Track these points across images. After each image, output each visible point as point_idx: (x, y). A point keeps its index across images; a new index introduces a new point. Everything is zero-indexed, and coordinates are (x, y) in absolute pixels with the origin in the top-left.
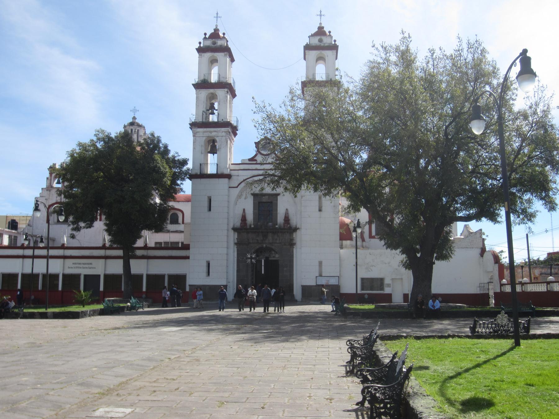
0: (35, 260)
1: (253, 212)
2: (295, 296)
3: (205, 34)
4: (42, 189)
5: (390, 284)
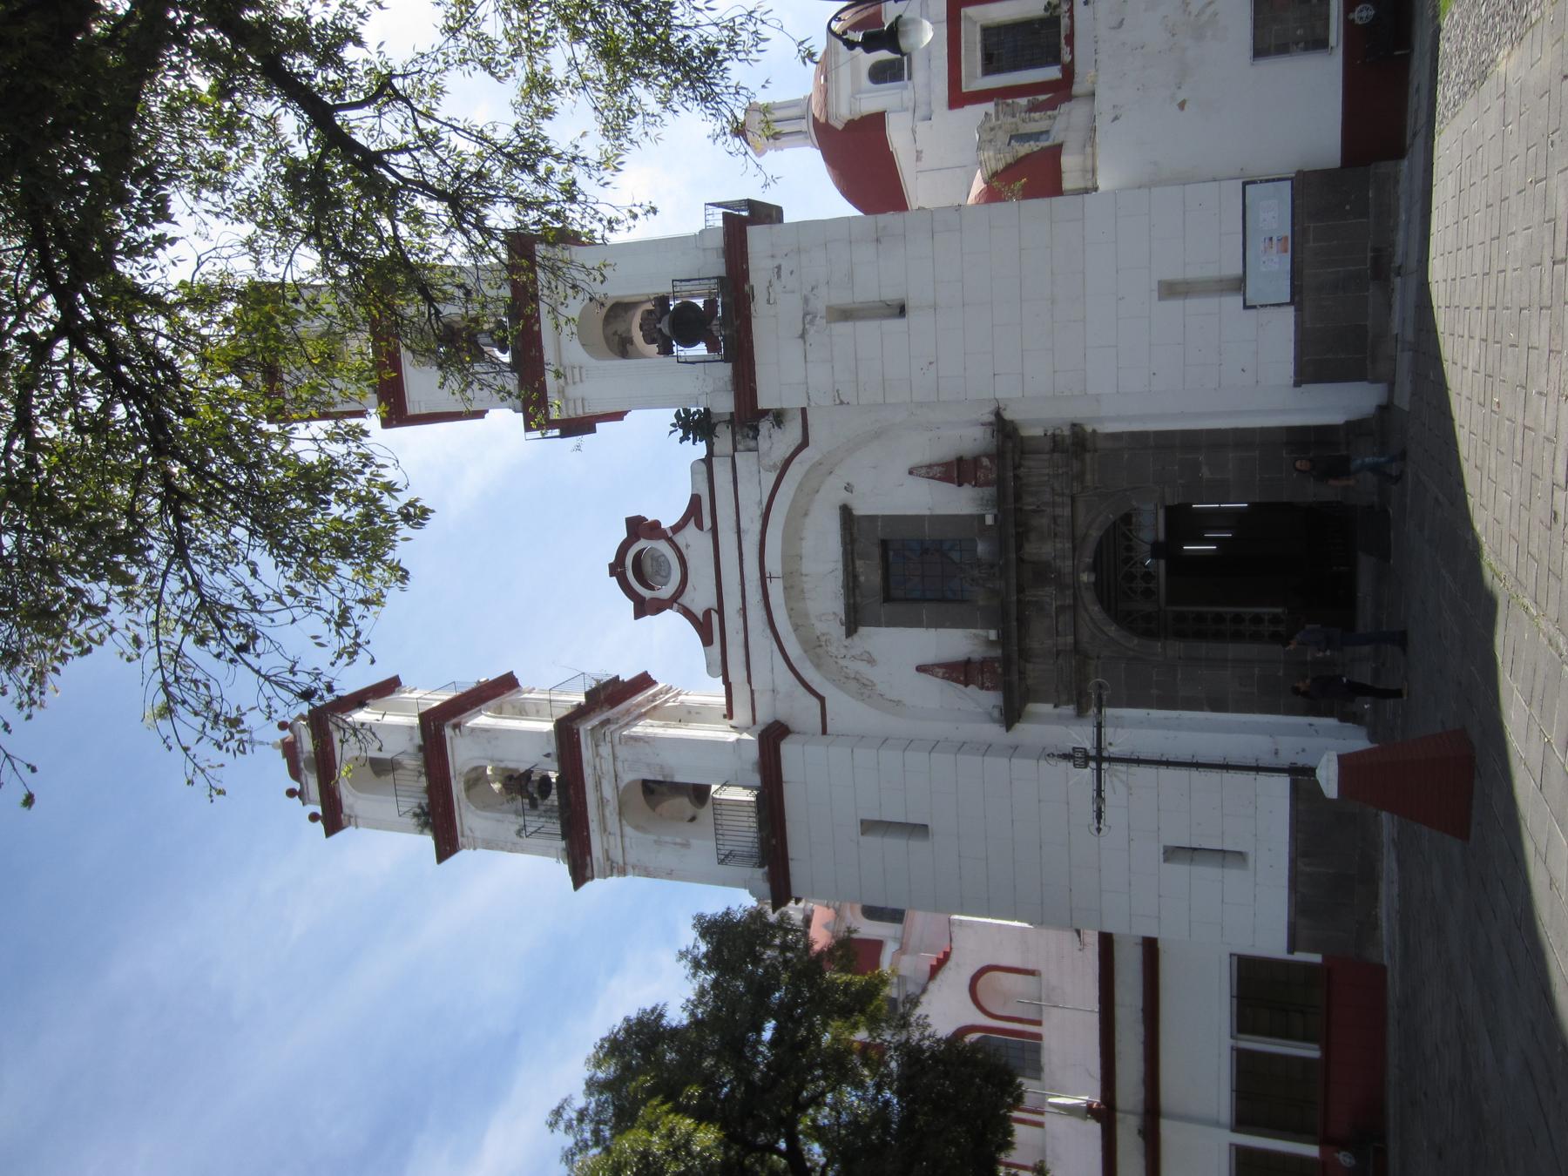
1: (929, 626)
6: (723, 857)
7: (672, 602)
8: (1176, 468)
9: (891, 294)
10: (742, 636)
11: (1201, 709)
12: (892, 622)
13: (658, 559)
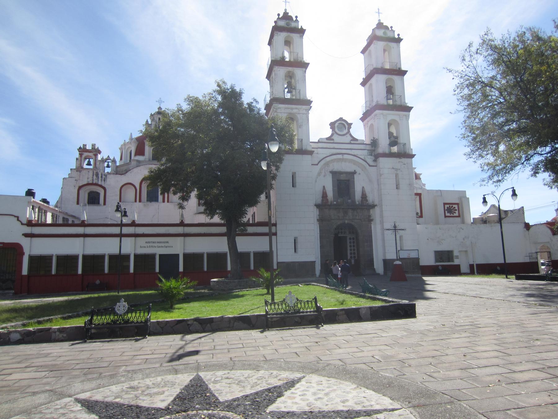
0: (123, 239)
1: (333, 189)
2: (376, 270)
3: (279, 15)
4: (71, 169)
5: (458, 256)
10: (329, 147)
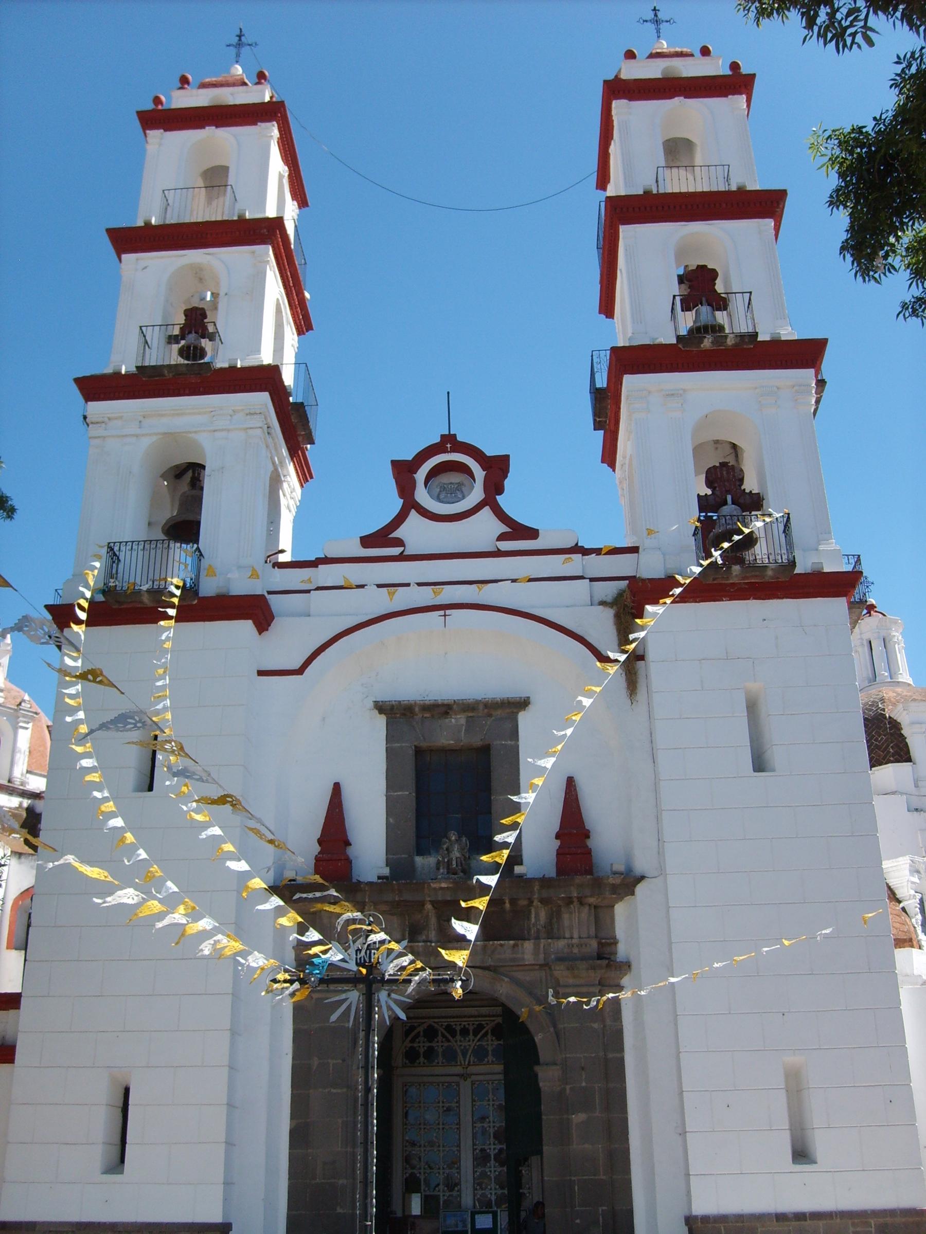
6: (116, 549)
7: (410, 505)
8: (584, 1084)
9: (777, 755)
11: (293, 1117)
12: (391, 755)
13: (456, 493)
